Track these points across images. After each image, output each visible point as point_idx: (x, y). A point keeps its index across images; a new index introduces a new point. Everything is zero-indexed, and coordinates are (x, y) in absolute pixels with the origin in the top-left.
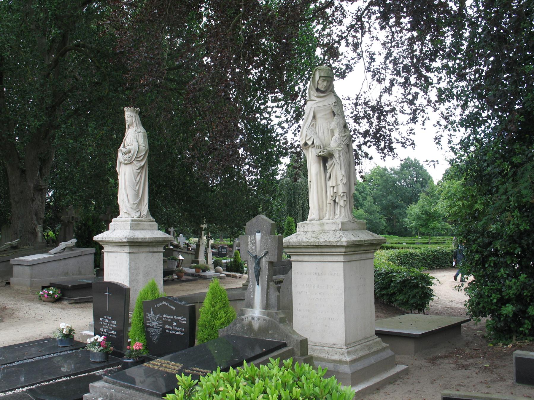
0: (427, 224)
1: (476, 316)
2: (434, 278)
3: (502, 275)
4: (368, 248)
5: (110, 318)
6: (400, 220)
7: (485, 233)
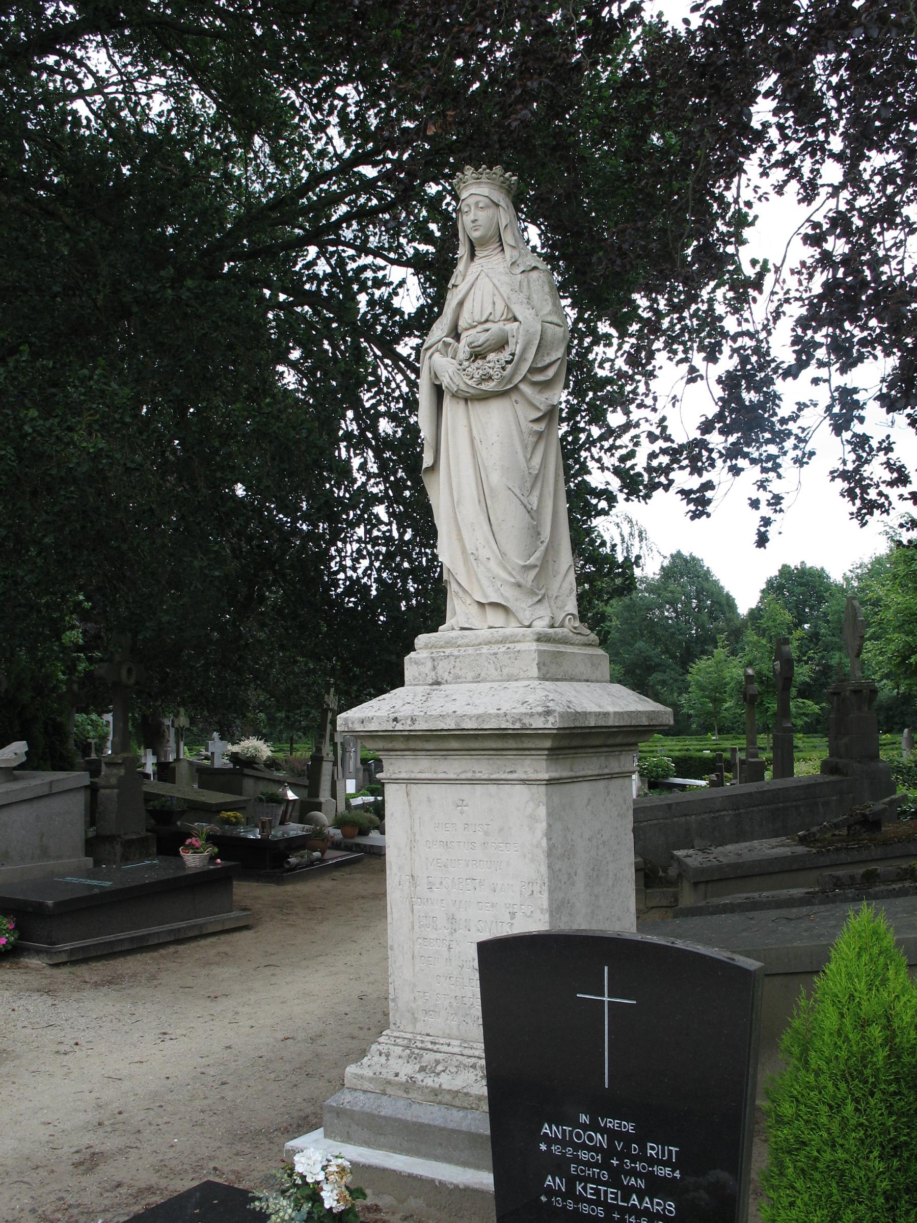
5: (630, 1127)
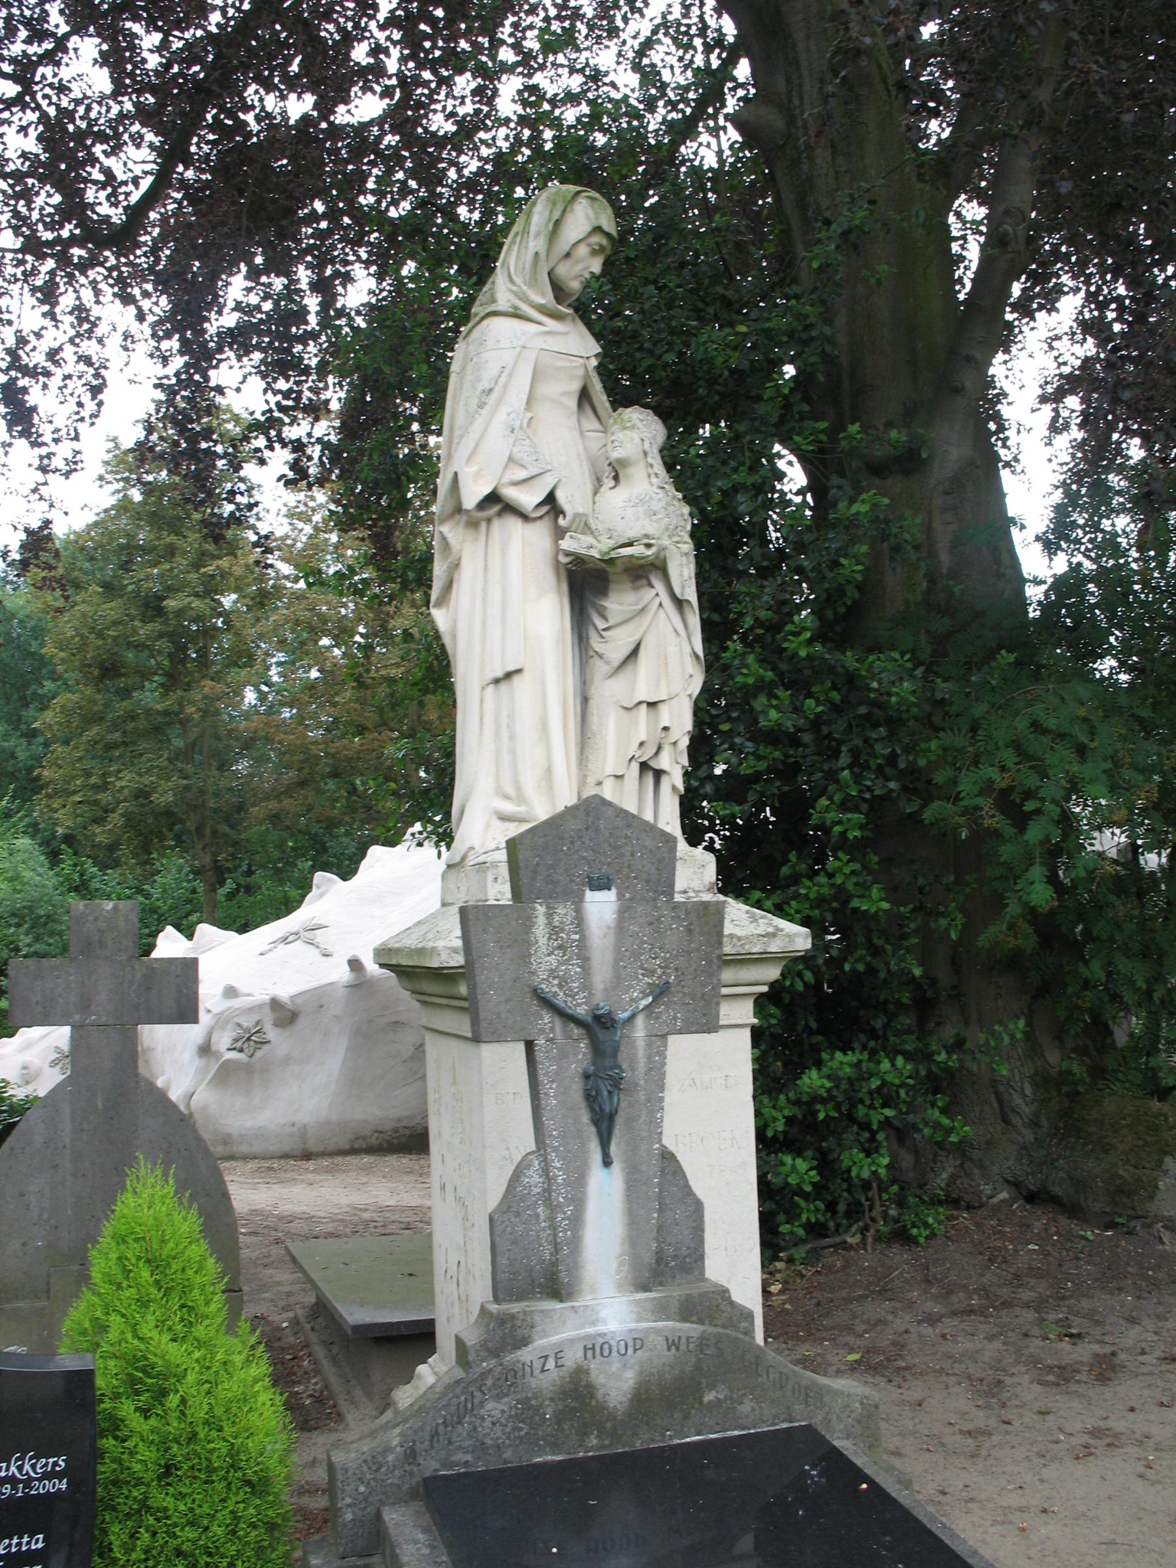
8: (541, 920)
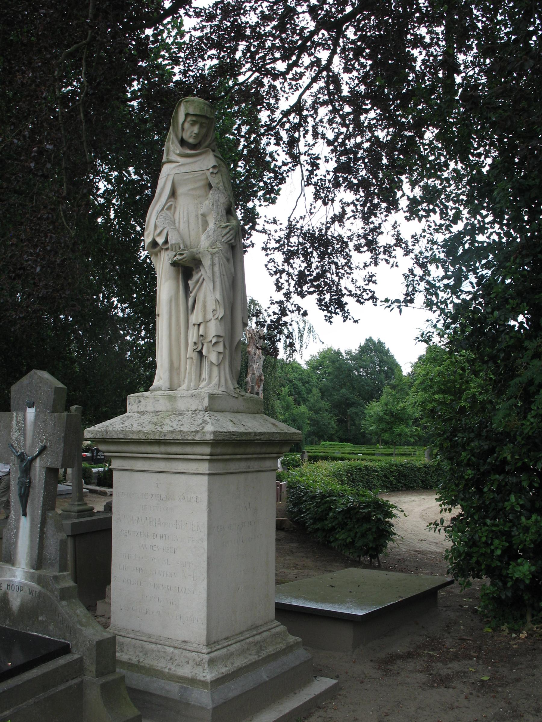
0: (391, 428)
1: (464, 576)
2: (396, 507)
3: (512, 508)
4: (264, 450)
6: (357, 422)
7: (484, 433)
8: (15, 419)
